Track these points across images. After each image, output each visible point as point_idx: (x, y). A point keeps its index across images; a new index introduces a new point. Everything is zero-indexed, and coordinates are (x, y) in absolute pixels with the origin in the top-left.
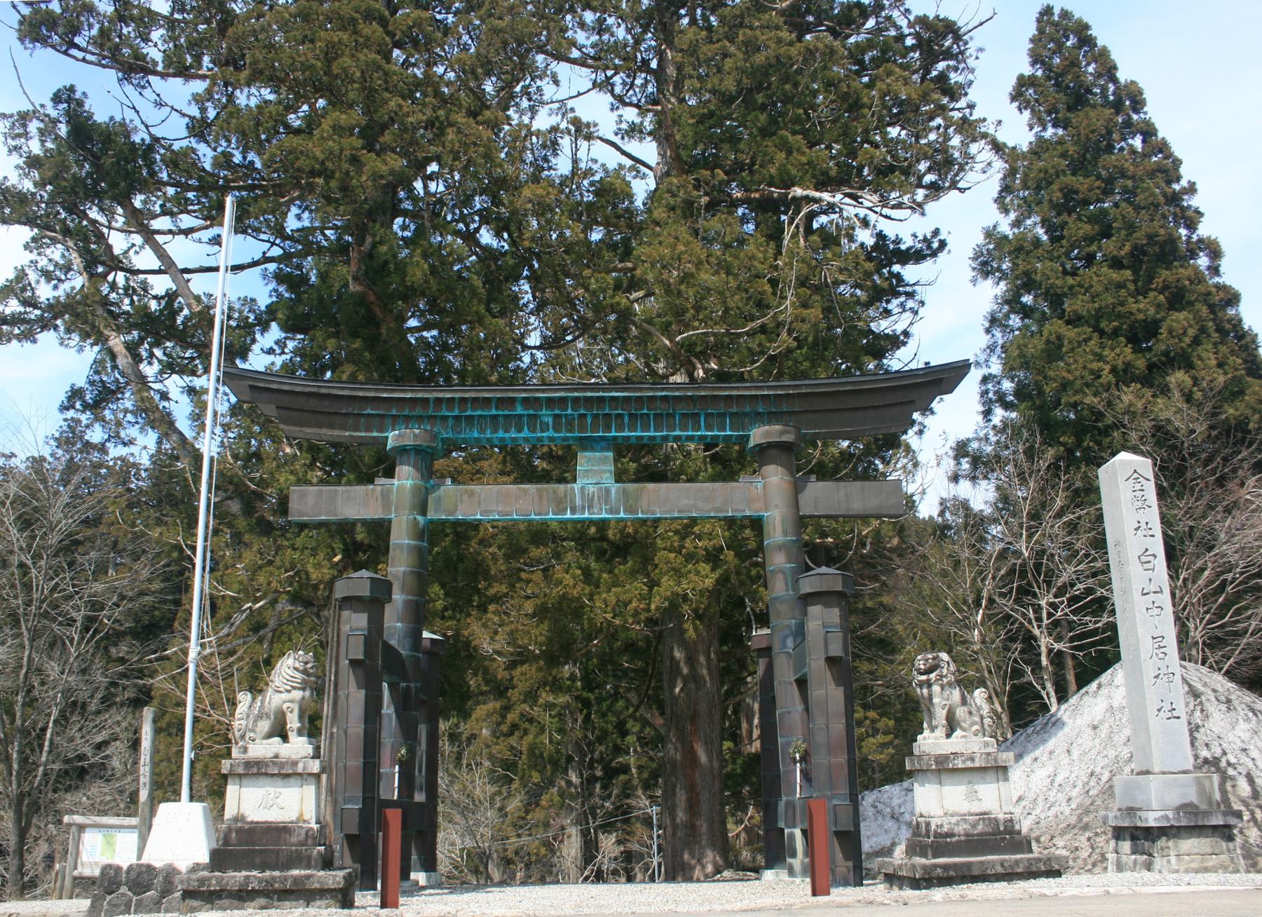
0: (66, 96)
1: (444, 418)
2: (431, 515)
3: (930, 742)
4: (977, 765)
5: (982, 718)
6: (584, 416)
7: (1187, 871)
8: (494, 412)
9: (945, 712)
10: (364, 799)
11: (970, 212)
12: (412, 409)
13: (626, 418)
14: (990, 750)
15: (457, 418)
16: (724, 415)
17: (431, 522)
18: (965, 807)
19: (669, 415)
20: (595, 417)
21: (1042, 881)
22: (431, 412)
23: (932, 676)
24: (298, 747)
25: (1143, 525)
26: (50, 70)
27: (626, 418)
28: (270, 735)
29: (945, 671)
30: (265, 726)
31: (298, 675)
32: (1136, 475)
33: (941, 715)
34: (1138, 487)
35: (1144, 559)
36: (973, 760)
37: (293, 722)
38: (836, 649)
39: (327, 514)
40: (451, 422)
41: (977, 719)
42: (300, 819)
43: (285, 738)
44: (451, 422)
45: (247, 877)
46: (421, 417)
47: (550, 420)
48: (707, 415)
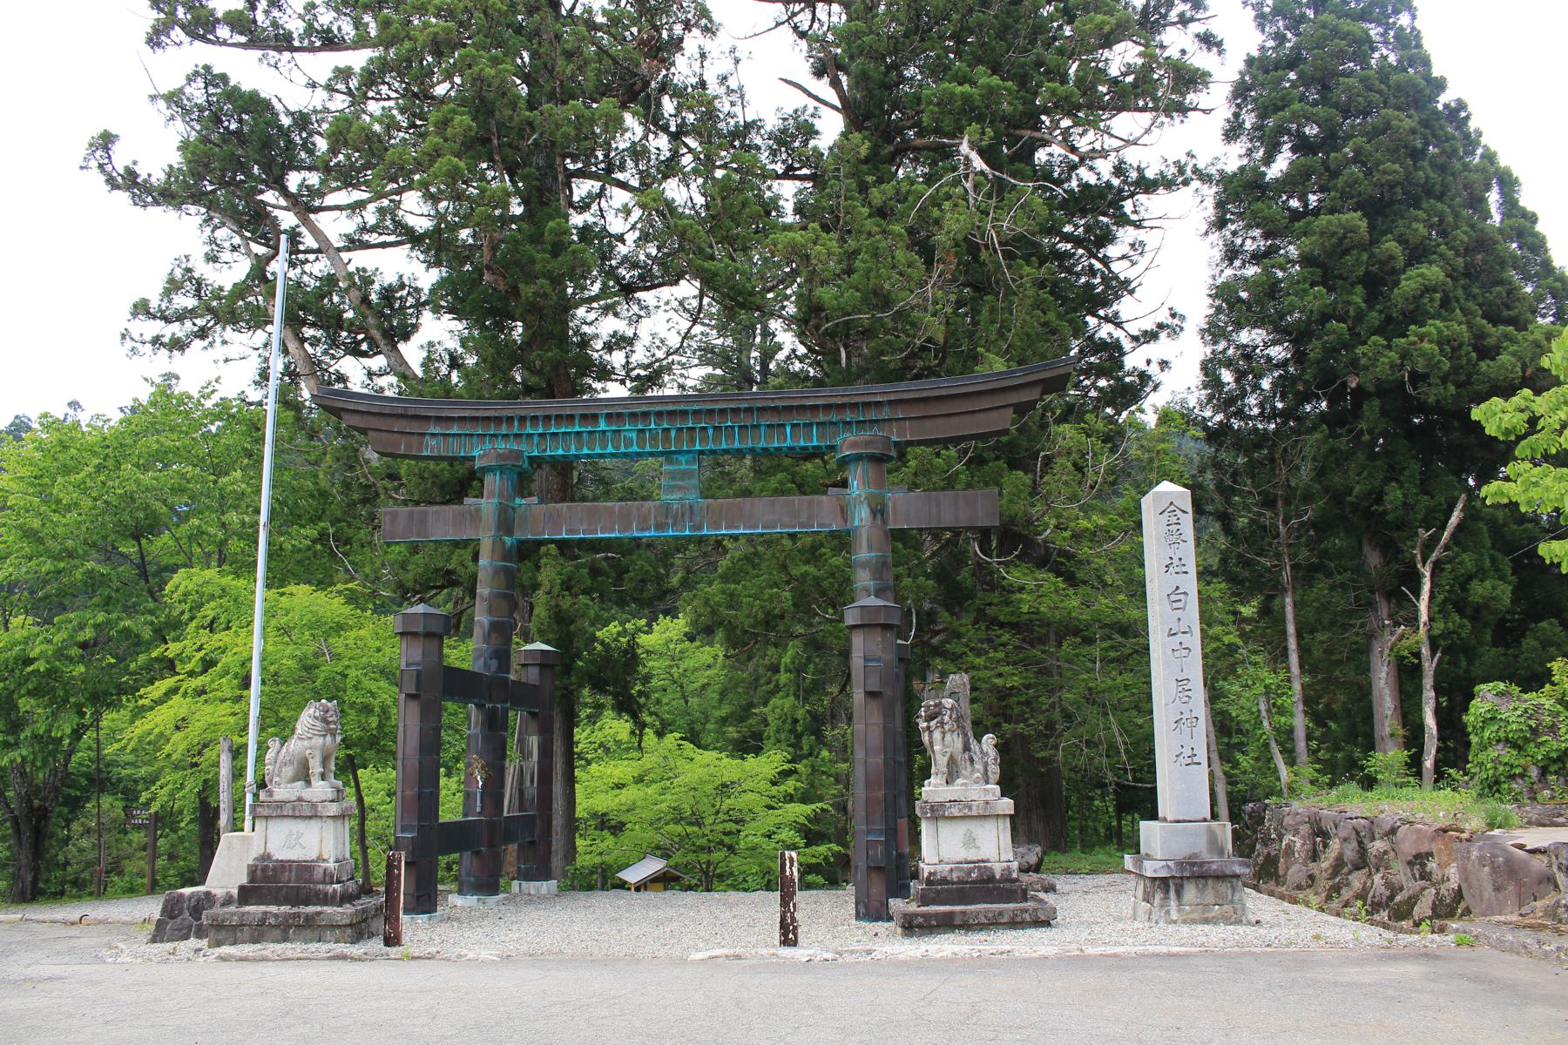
0: (210, 77)
1: (530, 436)
2: (519, 535)
3: (933, 789)
4: (974, 813)
5: (986, 765)
6: (668, 430)
7: (1185, 922)
8: (577, 429)
9: (946, 759)
10: (420, 828)
11: (1203, 136)
12: (498, 426)
13: (710, 432)
14: (990, 797)
15: (540, 435)
16: (811, 425)
17: (521, 542)
18: (960, 853)
19: (753, 426)
20: (680, 430)
21: (1011, 934)
22: (516, 431)
23: (933, 723)
24: (320, 790)
25: (1176, 562)
26: (184, 57)
27: (710, 432)
28: (294, 779)
29: (946, 718)
30: (289, 771)
31: (318, 723)
32: (1171, 508)
33: (940, 763)
34: (1174, 520)
35: (1173, 597)
36: (970, 808)
37: (316, 767)
38: (874, 686)
39: (419, 535)
40: (536, 439)
41: (979, 766)
42: (320, 859)
43: (308, 783)
44: (536, 439)
45: (265, 913)
46: (495, 436)
47: (634, 435)
48: (794, 426)
